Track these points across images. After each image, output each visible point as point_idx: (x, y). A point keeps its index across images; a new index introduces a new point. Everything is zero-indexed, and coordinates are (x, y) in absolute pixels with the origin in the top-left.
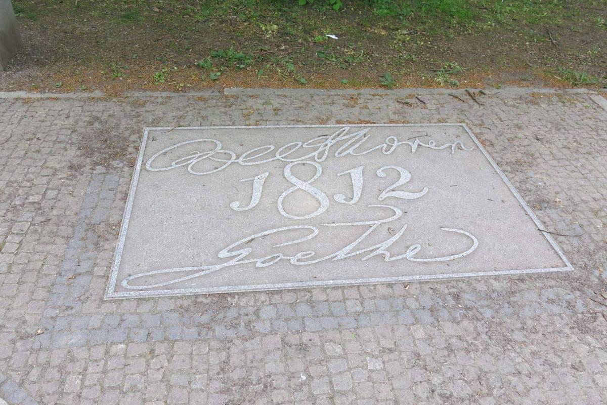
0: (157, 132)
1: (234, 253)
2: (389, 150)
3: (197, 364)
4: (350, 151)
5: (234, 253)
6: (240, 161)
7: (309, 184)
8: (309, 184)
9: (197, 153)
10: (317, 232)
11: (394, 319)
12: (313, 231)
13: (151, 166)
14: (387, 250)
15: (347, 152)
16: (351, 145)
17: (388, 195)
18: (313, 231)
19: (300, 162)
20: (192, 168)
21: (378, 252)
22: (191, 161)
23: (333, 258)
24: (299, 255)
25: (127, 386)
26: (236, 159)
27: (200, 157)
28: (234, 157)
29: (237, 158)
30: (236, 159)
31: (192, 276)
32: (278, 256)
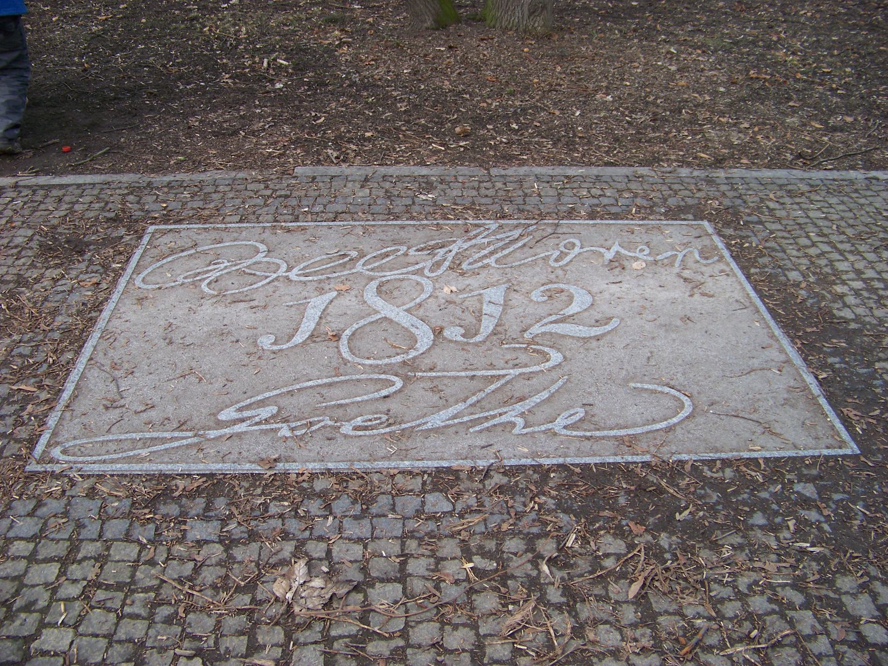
0: (37, 588)
1: (246, 414)
2: (562, 259)
3: (142, 576)
4: (491, 261)
5: (246, 414)
6: (292, 275)
7: (406, 310)
8: (406, 310)
9: (223, 263)
10: (399, 384)
11: (55, 205)
12: (393, 384)
13: (143, 280)
14: (522, 415)
15: (486, 261)
16: (492, 253)
17: (543, 329)
18: (393, 384)
19: (397, 277)
20: (682, 406)
21: (504, 419)
22: (207, 275)
23: (419, 425)
24: (359, 421)
25: (19, 602)
26: (286, 271)
27: (226, 267)
28: (284, 267)
29: (289, 269)
30: (286, 271)
31: (167, 446)
32: (323, 421)
